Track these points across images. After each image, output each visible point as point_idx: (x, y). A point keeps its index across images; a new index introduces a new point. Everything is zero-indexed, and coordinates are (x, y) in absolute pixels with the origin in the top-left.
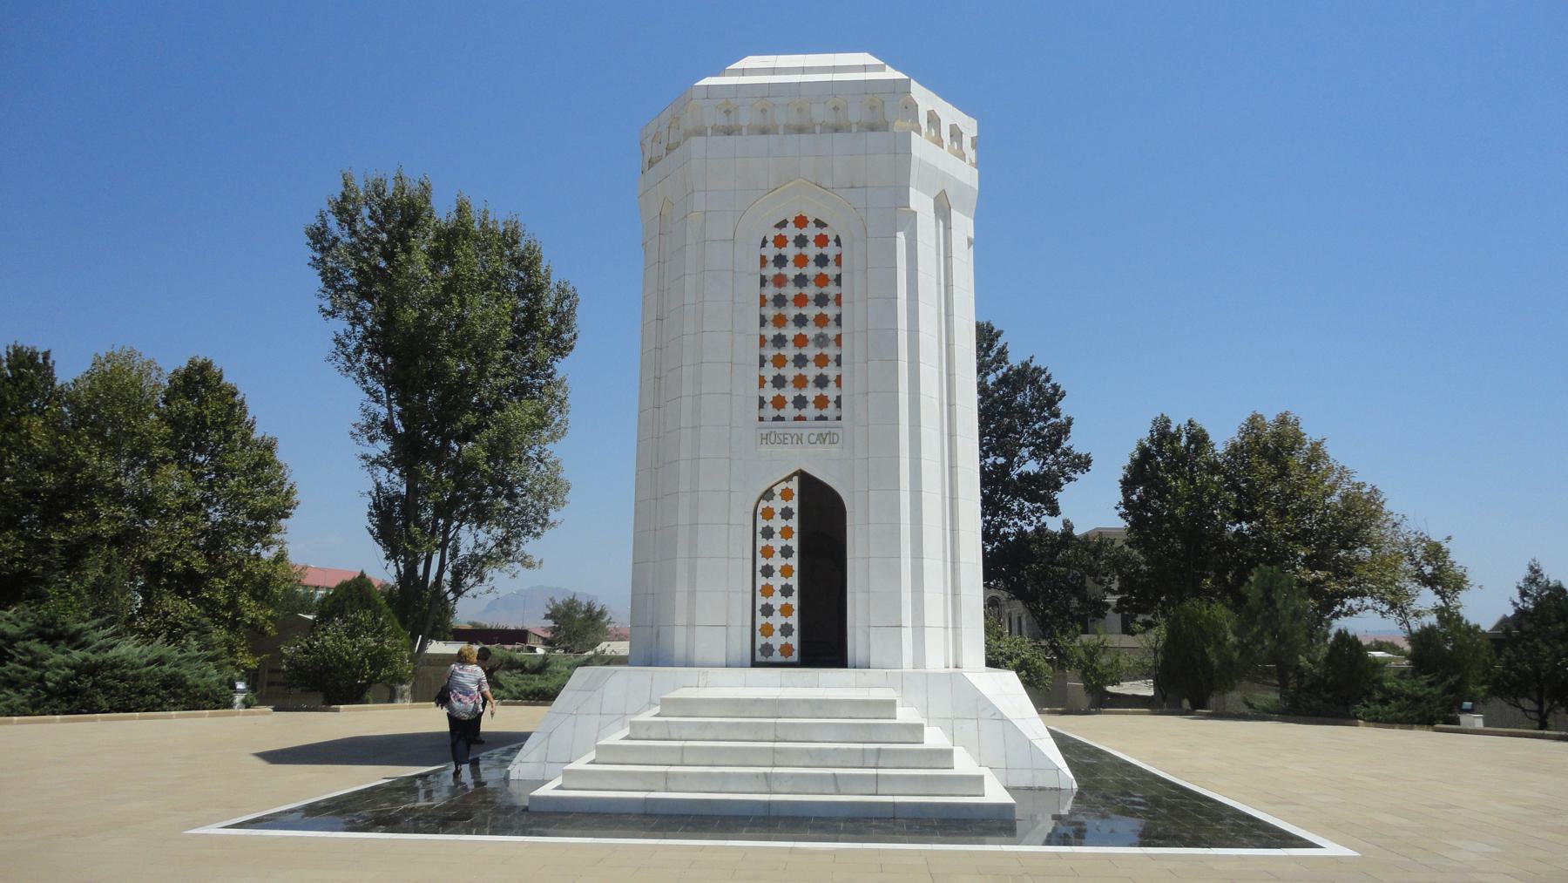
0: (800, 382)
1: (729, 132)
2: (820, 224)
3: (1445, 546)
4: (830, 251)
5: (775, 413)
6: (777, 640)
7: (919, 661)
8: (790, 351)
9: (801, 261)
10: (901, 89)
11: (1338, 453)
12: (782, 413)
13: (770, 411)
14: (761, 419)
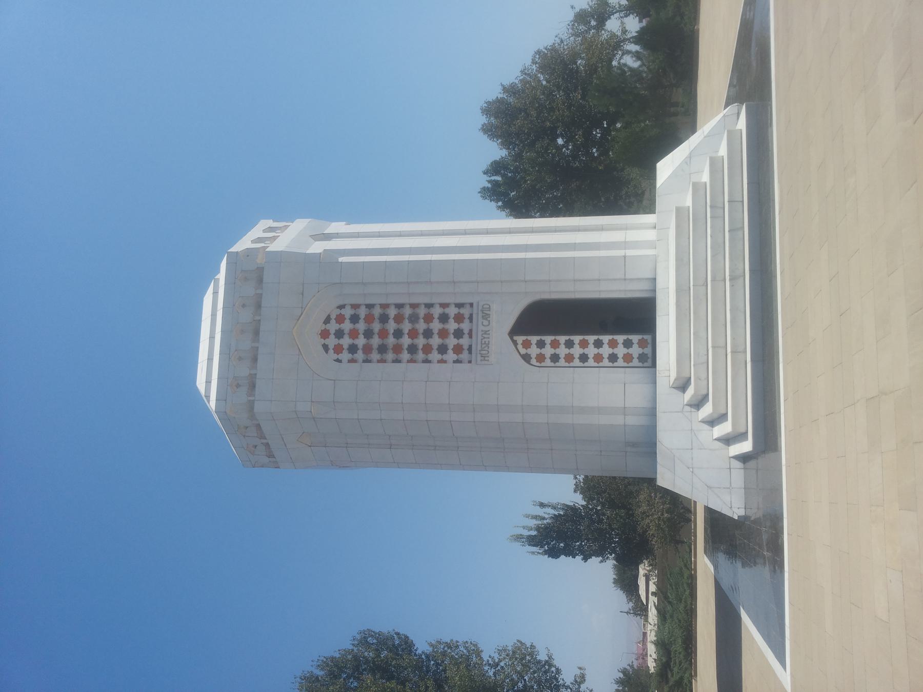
0: (443, 334)
1: (253, 386)
2: (327, 320)
3: (577, 10)
4: (348, 312)
5: (466, 352)
6: (635, 351)
7: (651, 245)
8: (421, 341)
9: (354, 334)
10: (234, 260)
11: (512, 76)
12: (466, 347)
13: (465, 356)
14: (470, 362)
